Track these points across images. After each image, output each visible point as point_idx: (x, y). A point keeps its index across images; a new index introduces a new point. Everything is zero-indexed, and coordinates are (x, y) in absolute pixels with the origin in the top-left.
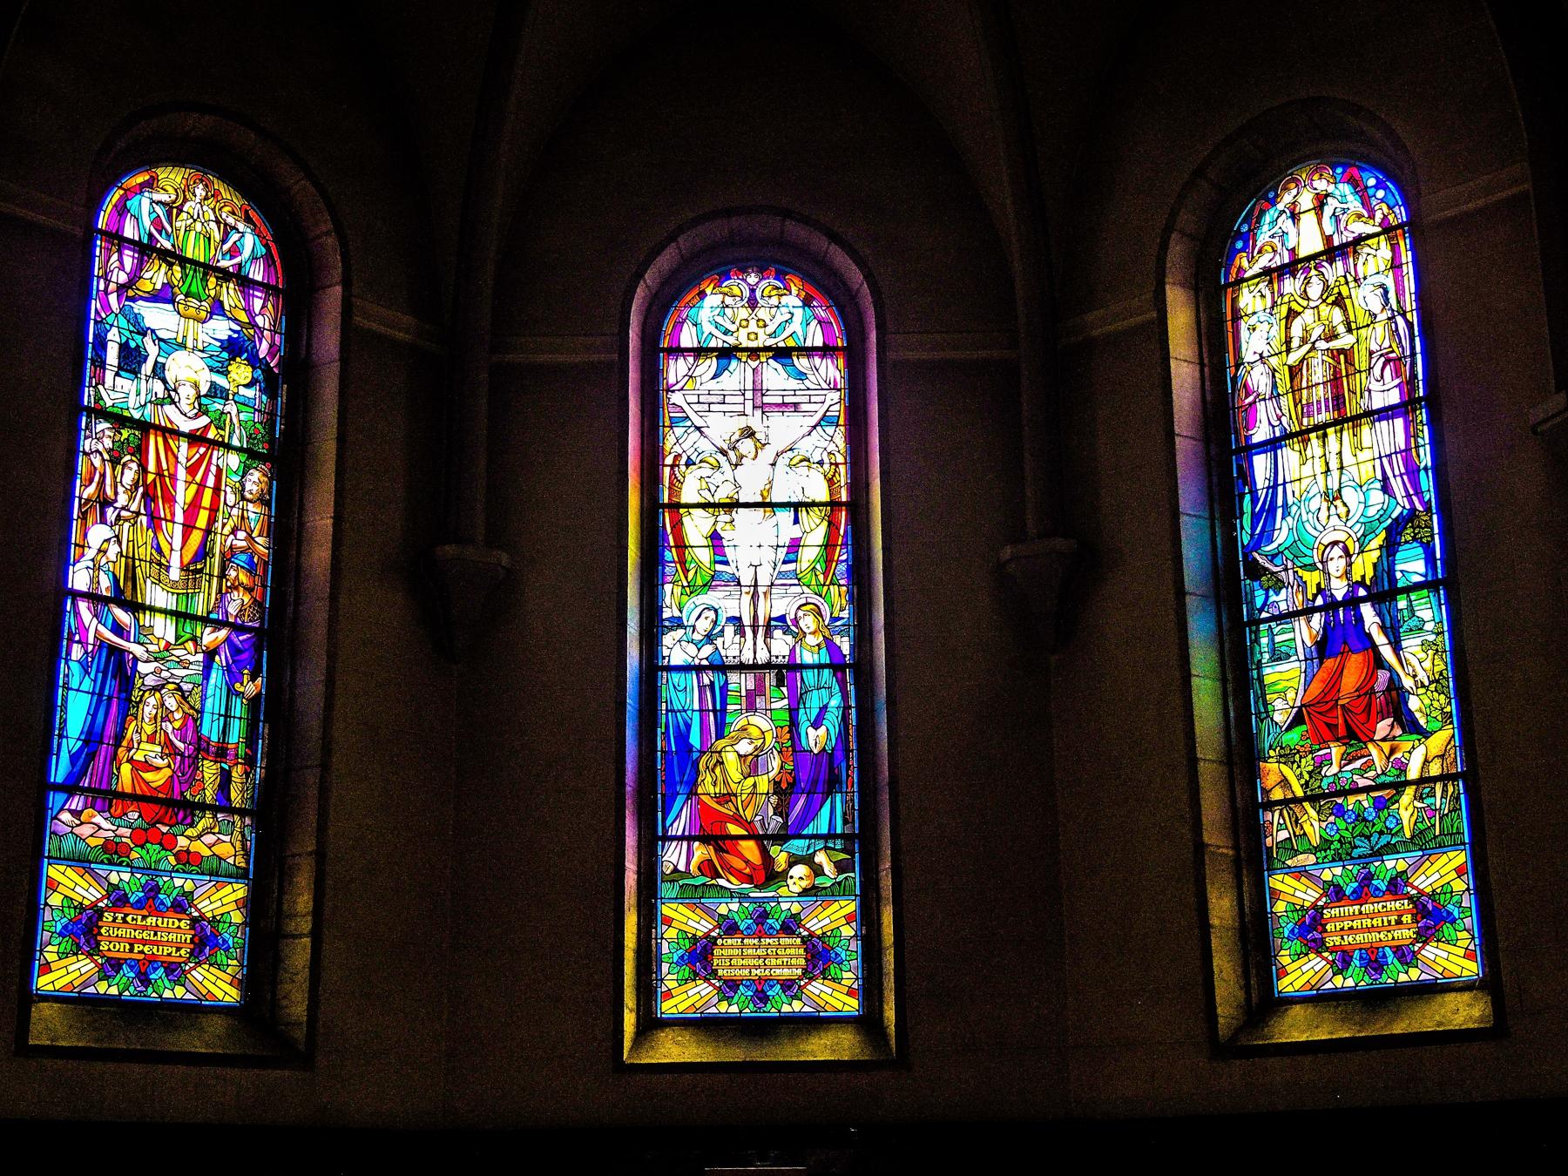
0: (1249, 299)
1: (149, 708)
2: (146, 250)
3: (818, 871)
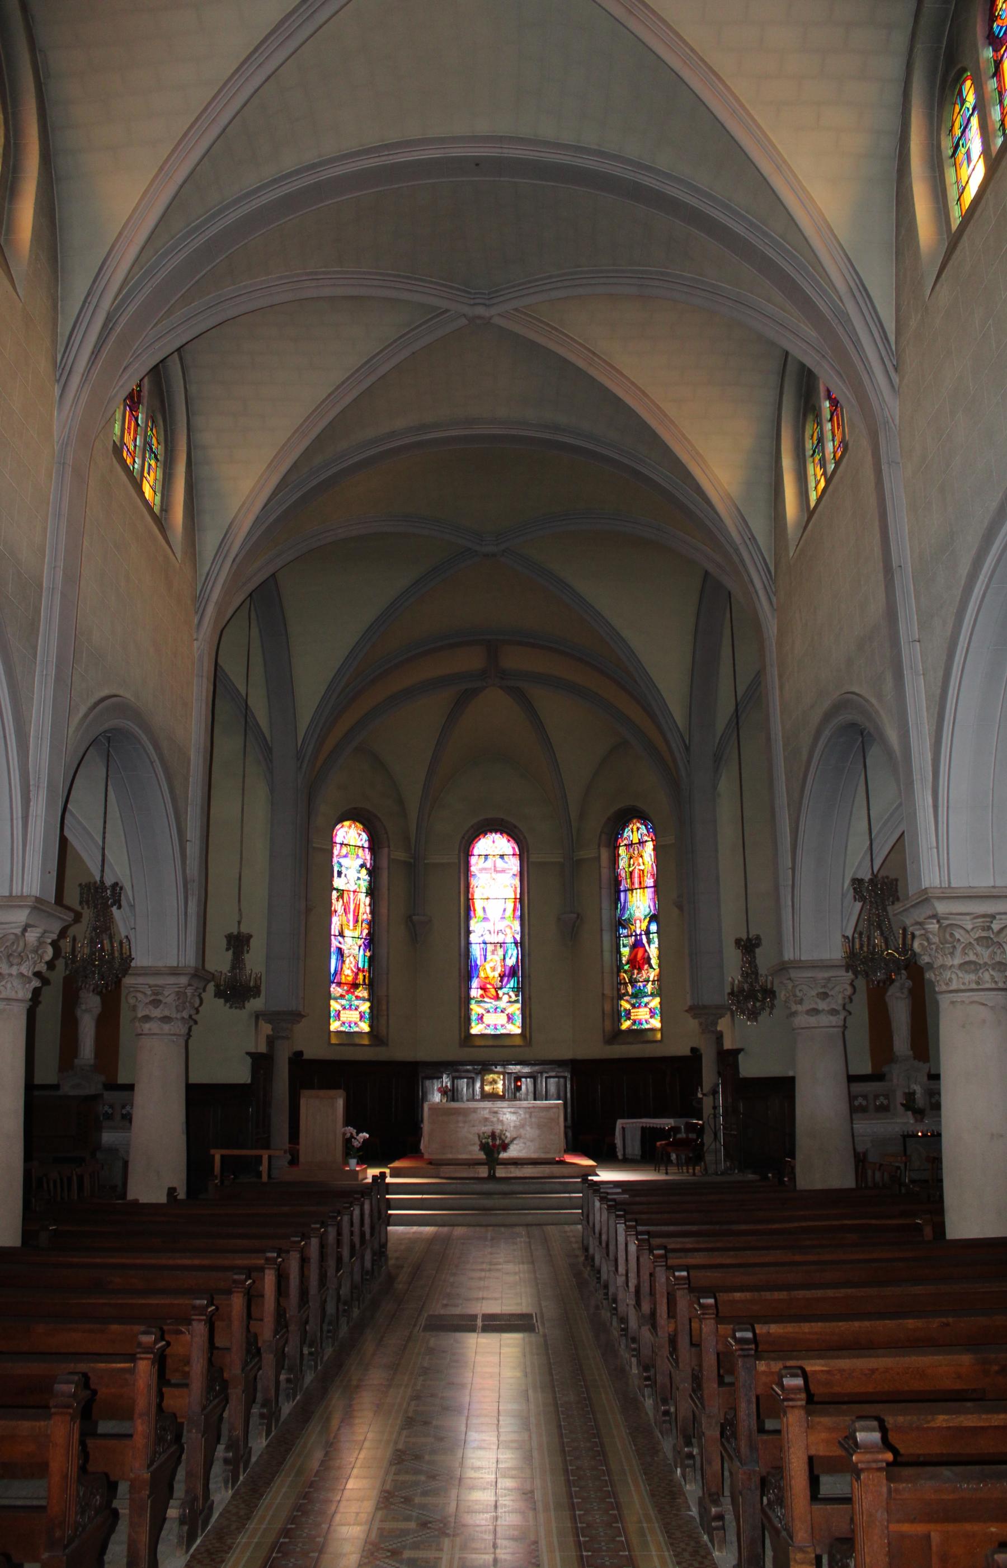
0: (622, 851)
1: (347, 961)
2: (342, 844)
3: (510, 997)
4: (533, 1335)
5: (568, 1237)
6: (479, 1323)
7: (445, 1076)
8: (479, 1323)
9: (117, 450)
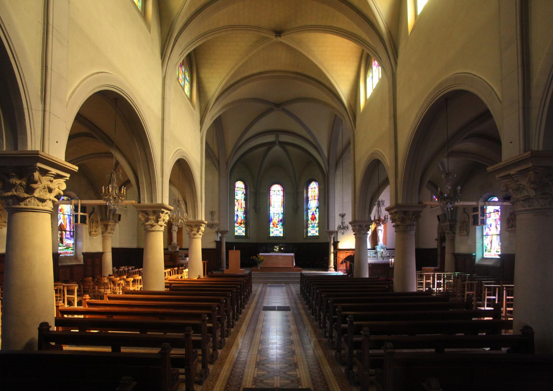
8: (276, 308)
9: (178, 79)
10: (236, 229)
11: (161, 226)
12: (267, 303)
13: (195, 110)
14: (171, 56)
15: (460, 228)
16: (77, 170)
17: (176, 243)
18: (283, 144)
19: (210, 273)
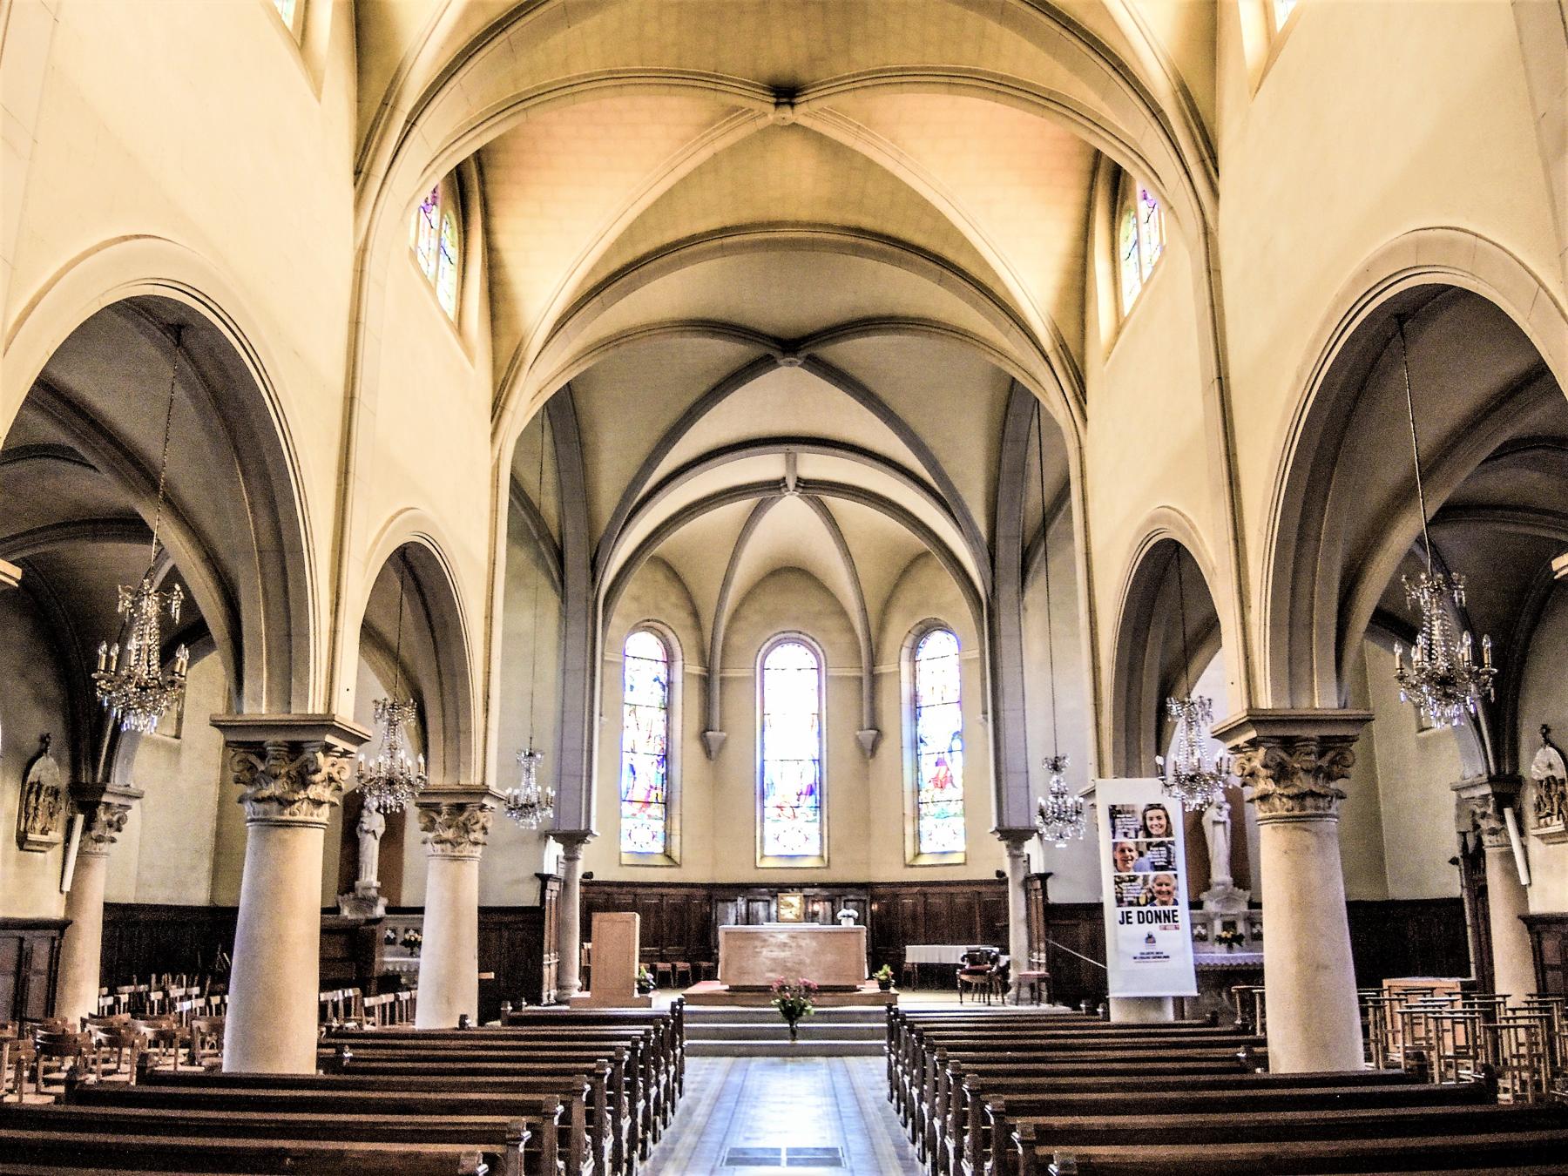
4: (839, 1169)
5: (871, 1069)
6: (784, 1157)
7: (740, 899)
8: (784, 1157)
9: (413, 254)
10: (626, 825)
11: (318, 803)
12: (747, 1135)
13: (473, 365)
14: (382, 198)
15: (1538, 807)
16: (17, 582)
17: (376, 884)
18: (810, 488)
19: (510, 1008)
